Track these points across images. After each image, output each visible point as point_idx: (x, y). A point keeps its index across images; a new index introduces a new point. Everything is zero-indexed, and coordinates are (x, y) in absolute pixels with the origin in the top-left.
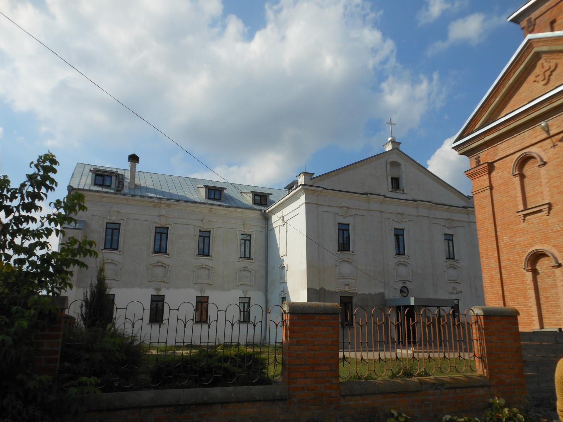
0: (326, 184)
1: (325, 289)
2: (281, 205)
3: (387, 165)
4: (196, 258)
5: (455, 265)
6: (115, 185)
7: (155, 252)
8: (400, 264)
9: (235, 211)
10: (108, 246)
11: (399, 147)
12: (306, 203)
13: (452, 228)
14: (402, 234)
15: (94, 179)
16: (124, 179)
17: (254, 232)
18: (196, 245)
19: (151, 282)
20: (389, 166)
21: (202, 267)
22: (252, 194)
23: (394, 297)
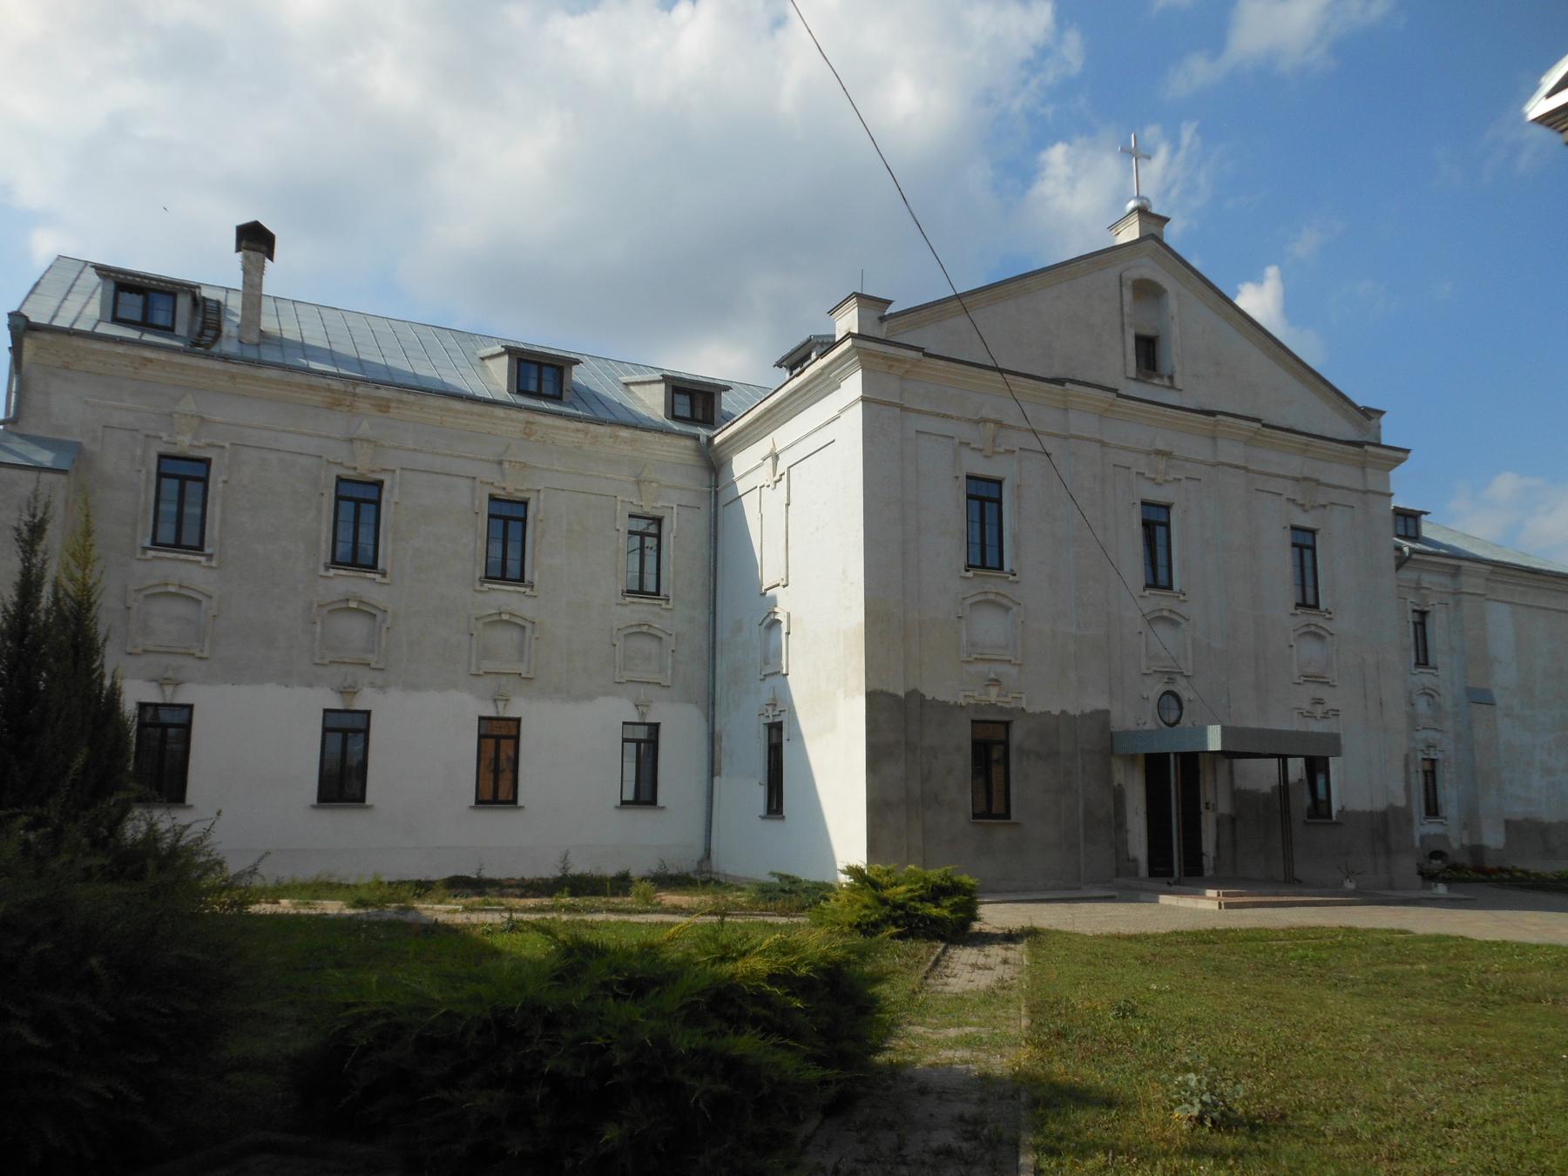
0: (928, 338)
1: (922, 696)
2: (769, 415)
3: (1125, 291)
4: (478, 588)
5: (1321, 627)
6: (190, 331)
7: (335, 563)
8: (1155, 619)
9: (611, 437)
10: (167, 533)
11: (1162, 233)
12: (864, 399)
13: (1313, 507)
14: (1164, 519)
15: (110, 302)
16: (222, 313)
17: (672, 508)
18: (479, 544)
19: (324, 665)
20: (1128, 295)
21: (500, 621)
22: (664, 385)
23: (1138, 725)
